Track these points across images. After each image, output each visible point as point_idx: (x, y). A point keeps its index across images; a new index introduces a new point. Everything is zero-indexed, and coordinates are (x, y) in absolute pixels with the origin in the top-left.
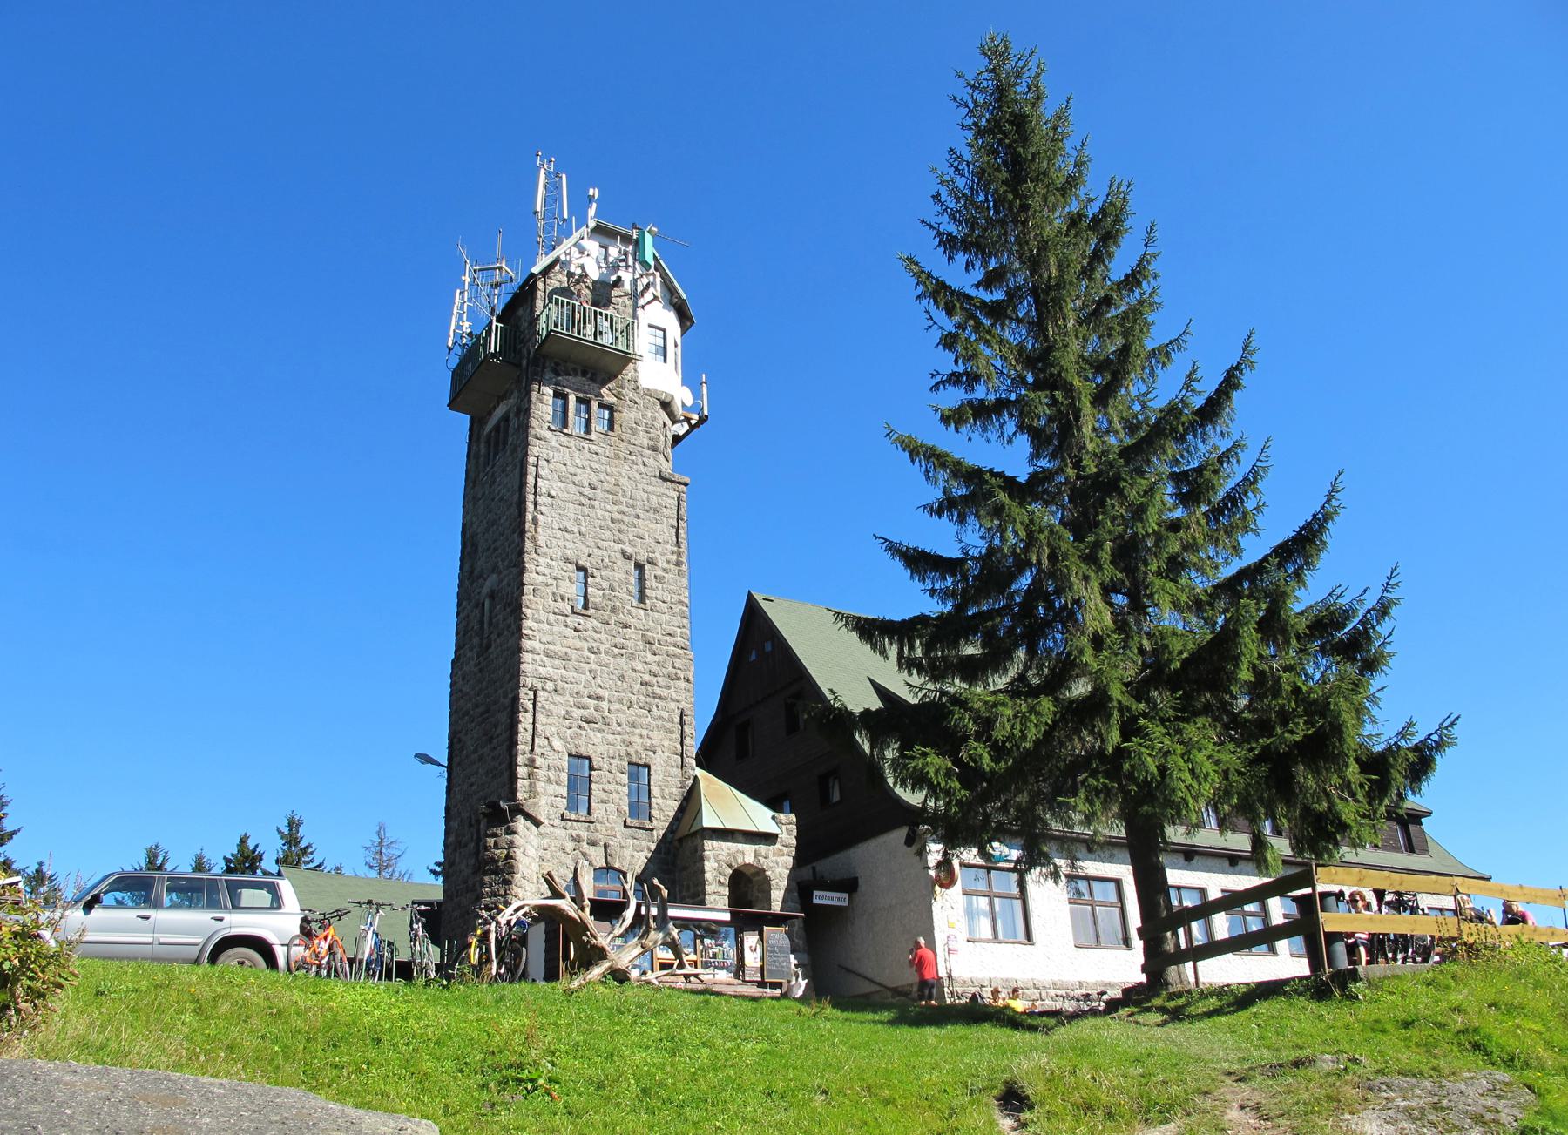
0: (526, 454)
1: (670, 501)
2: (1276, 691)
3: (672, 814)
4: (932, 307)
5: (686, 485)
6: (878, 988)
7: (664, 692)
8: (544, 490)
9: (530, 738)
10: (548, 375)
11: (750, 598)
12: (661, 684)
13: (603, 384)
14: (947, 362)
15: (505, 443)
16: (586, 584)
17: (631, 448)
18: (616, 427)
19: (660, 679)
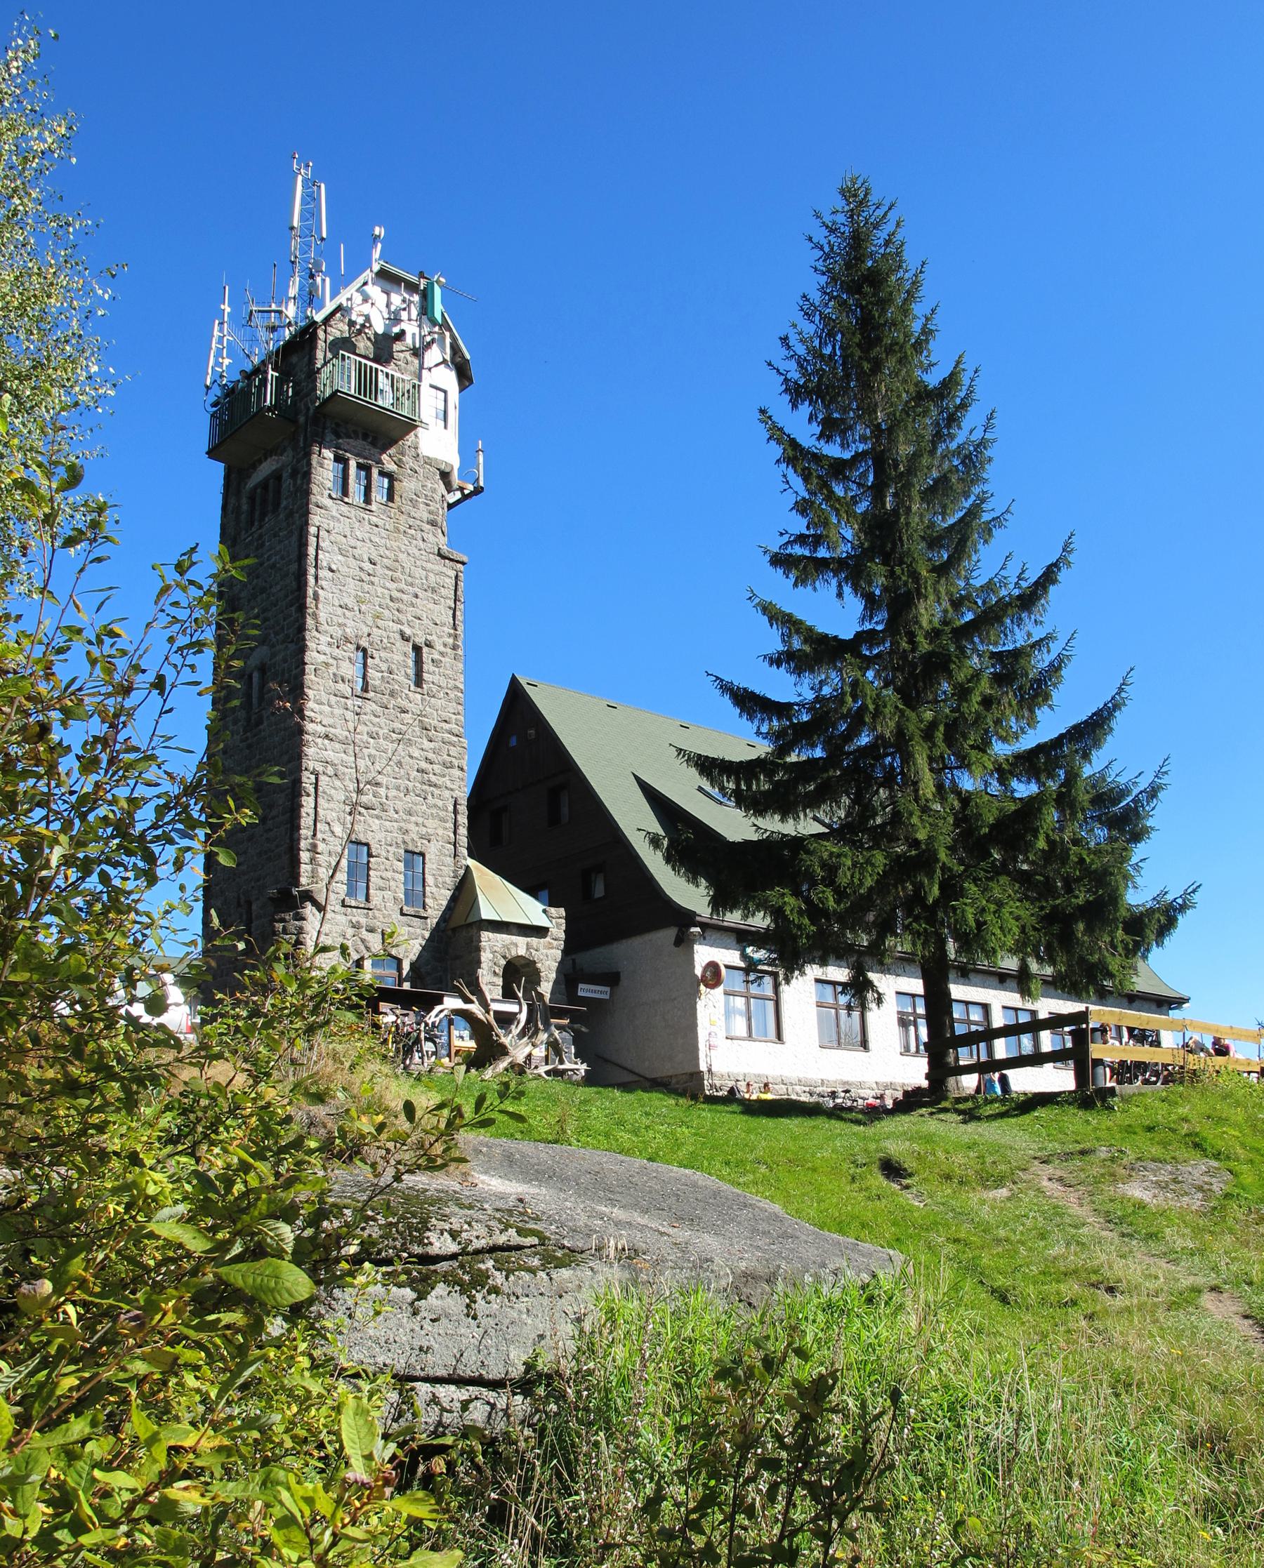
0: (307, 524)
1: (448, 580)
2: (1064, 859)
3: (445, 903)
4: (790, 471)
5: (463, 563)
6: (637, 1078)
7: (439, 781)
8: (325, 564)
9: (312, 823)
10: (329, 437)
11: (514, 681)
12: (437, 771)
13: (384, 450)
14: (799, 525)
15: (277, 505)
16: (365, 665)
17: (411, 521)
18: (397, 498)
19: (435, 767)
